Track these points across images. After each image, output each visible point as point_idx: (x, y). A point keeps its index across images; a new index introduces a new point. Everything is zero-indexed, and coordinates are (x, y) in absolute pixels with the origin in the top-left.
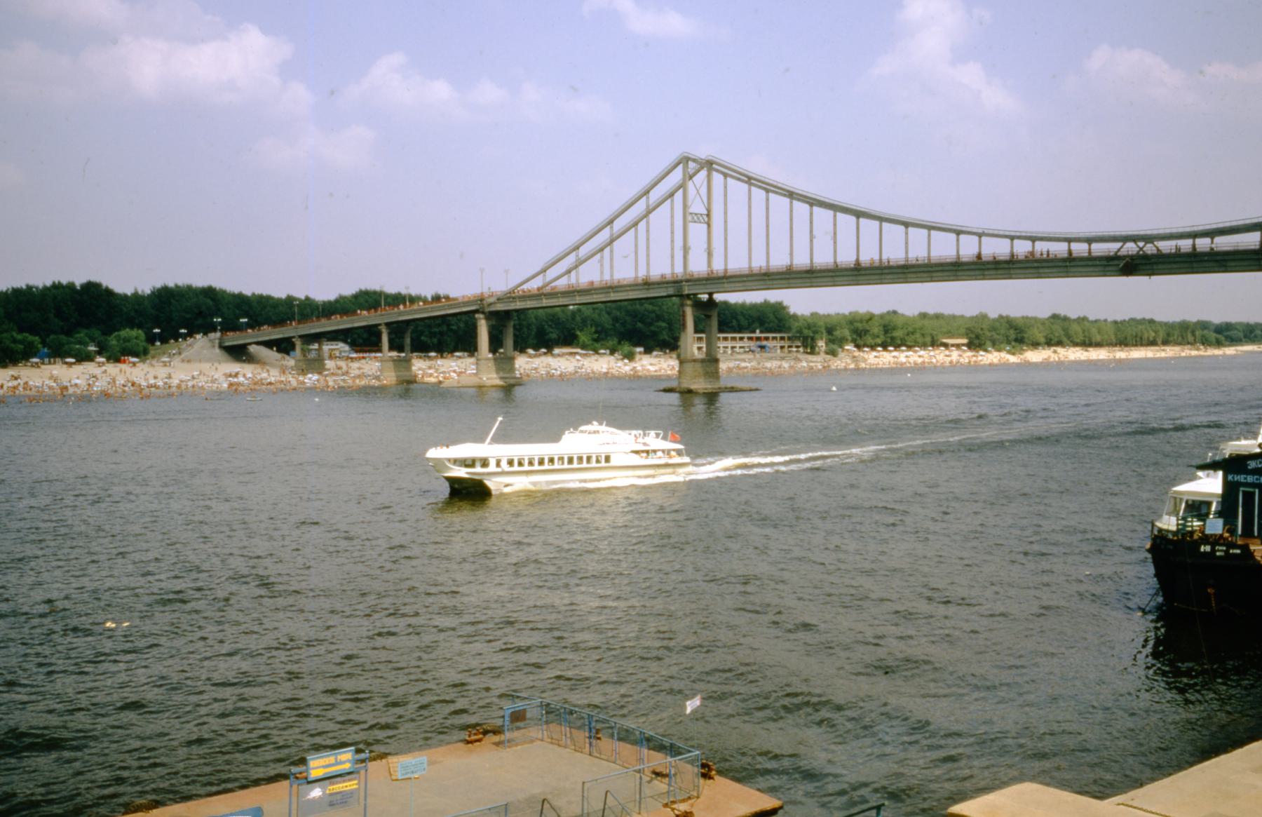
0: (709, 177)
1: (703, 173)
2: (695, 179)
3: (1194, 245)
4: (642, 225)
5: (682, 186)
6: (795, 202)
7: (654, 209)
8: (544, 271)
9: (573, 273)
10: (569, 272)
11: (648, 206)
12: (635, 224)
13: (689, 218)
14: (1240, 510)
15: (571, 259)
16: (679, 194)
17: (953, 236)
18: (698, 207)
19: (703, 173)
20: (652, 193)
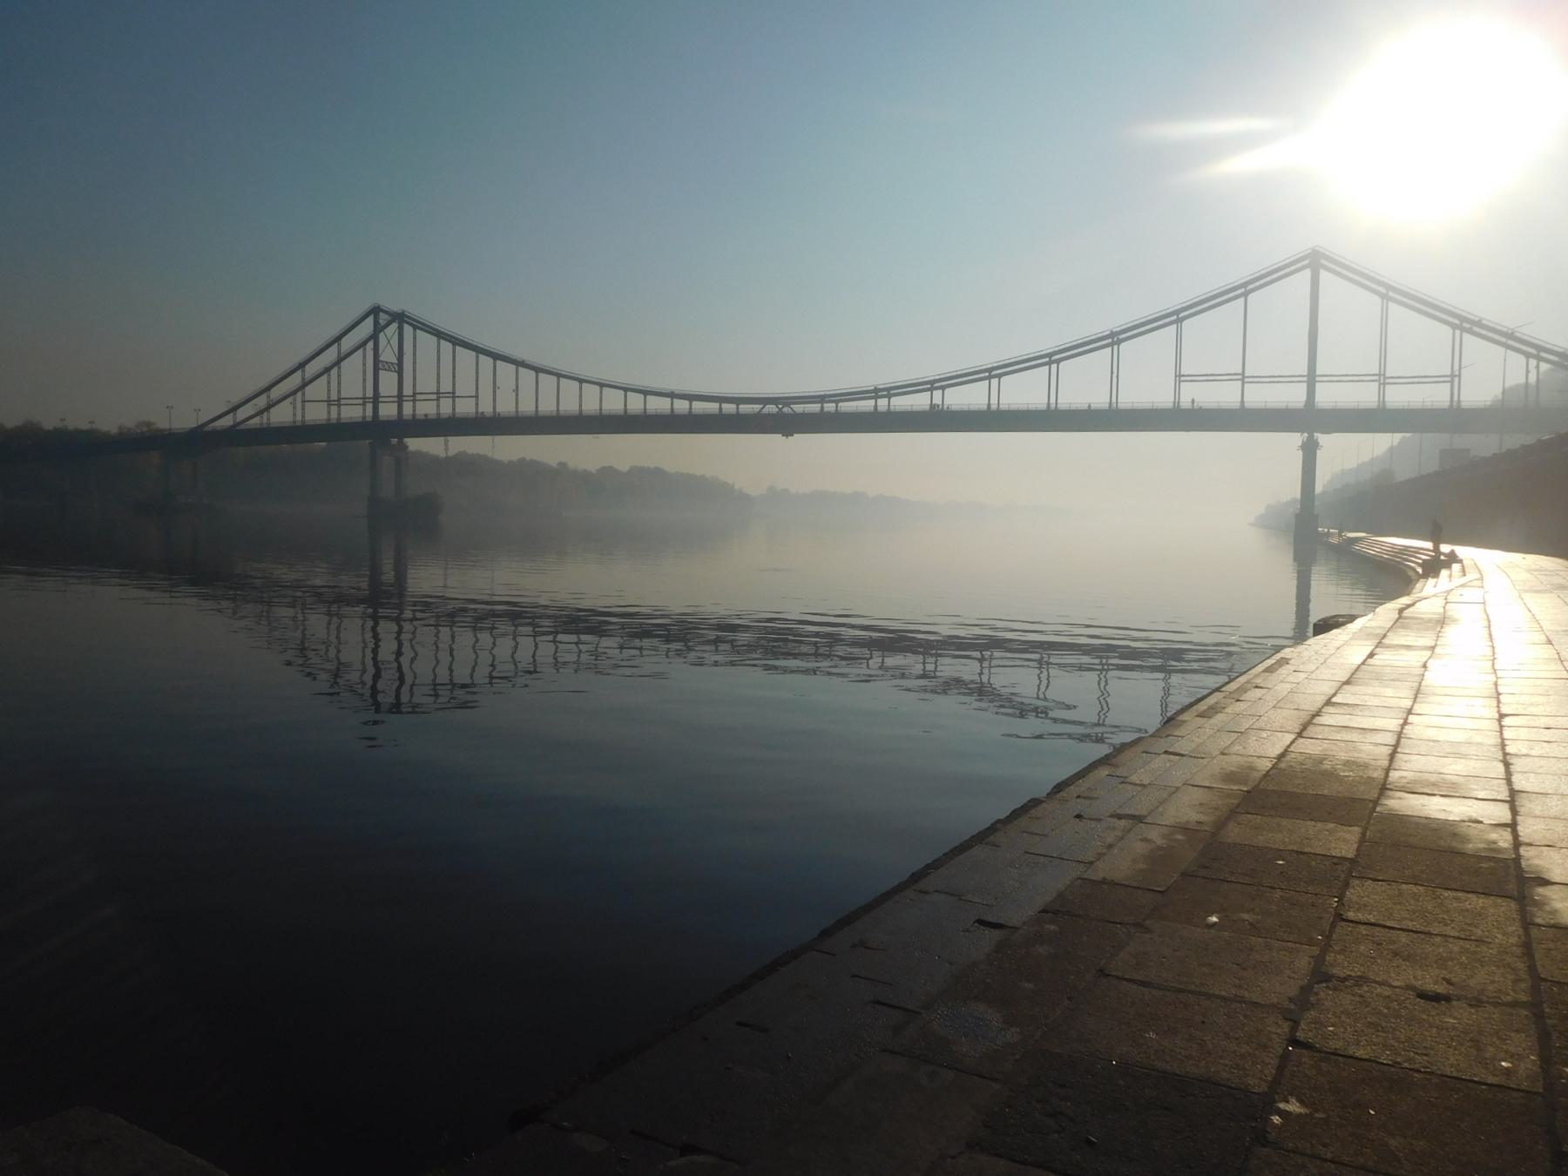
0: (401, 329)
1: (395, 326)
3: (720, 409)
4: (334, 372)
5: (374, 337)
6: (442, 341)
7: (311, 381)
10: (260, 413)
15: (261, 401)
16: (370, 345)
17: (598, 388)
18: (388, 355)
19: (395, 326)
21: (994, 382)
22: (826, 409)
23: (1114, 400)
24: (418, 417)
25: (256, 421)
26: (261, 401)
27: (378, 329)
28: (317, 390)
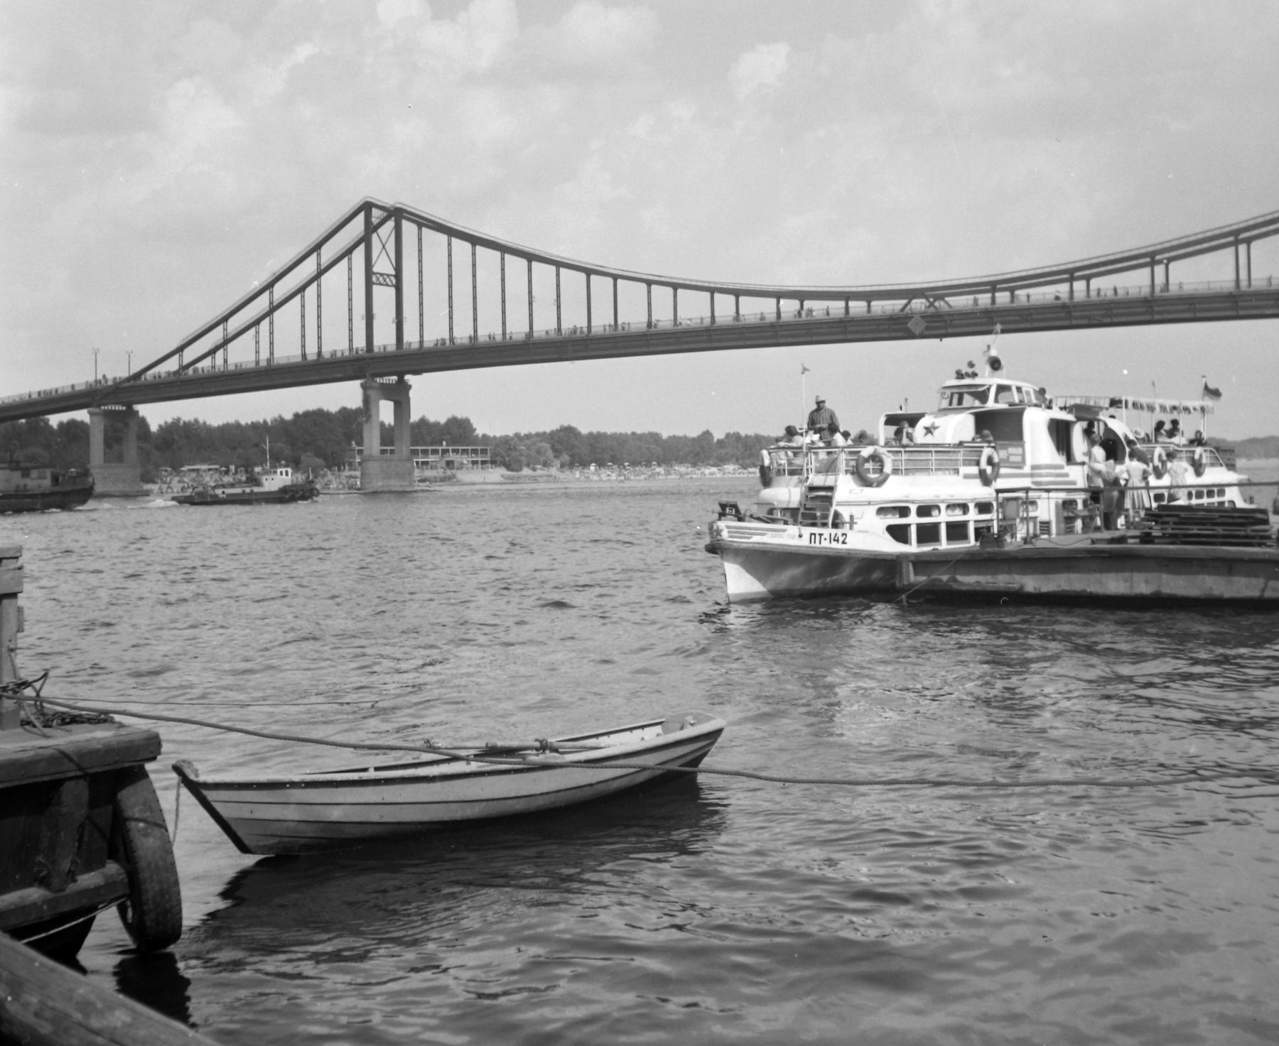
1: (390, 224)
2: (380, 231)
5: (366, 239)
8: (180, 349)
9: (220, 354)
10: (212, 352)
11: (271, 303)
12: (302, 290)
13: (374, 279)
14: (43, 935)
15: (216, 336)
16: (359, 254)
18: (383, 265)
19: (390, 224)
20: (277, 286)
21: (1242, 248)
22: (852, 311)
23: (1243, 275)
24: (458, 342)
25: (206, 363)
26: (216, 336)
27: (371, 229)
28: (287, 317)
